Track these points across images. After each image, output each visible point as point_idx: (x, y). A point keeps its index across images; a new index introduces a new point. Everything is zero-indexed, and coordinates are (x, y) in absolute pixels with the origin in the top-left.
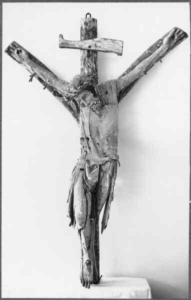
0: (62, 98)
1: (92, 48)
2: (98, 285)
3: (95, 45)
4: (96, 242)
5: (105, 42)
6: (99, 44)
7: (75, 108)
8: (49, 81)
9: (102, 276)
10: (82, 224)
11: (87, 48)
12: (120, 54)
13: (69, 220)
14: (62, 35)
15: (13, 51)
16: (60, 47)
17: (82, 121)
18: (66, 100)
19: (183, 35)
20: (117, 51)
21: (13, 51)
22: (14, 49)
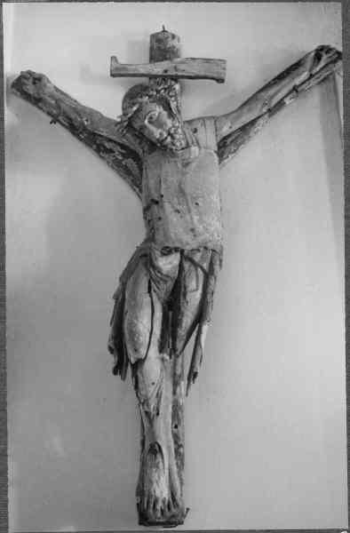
0: (112, 154)
1: (169, 73)
2: (181, 436)
3: (175, 68)
4: (176, 427)
5: (195, 64)
6: (182, 67)
7: (135, 171)
8: (87, 120)
9: (188, 509)
10: (92, 123)
11: (160, 73)
12: (220, 80)
13: (111, 360)
14: (115, 57)
15: (26, 81)
16: (113, 75)
17: (169, 465)
18: (120, 158)
19: (336, 56)
20: (215, 76)
21: (26, 81)
22: (31, 88)
